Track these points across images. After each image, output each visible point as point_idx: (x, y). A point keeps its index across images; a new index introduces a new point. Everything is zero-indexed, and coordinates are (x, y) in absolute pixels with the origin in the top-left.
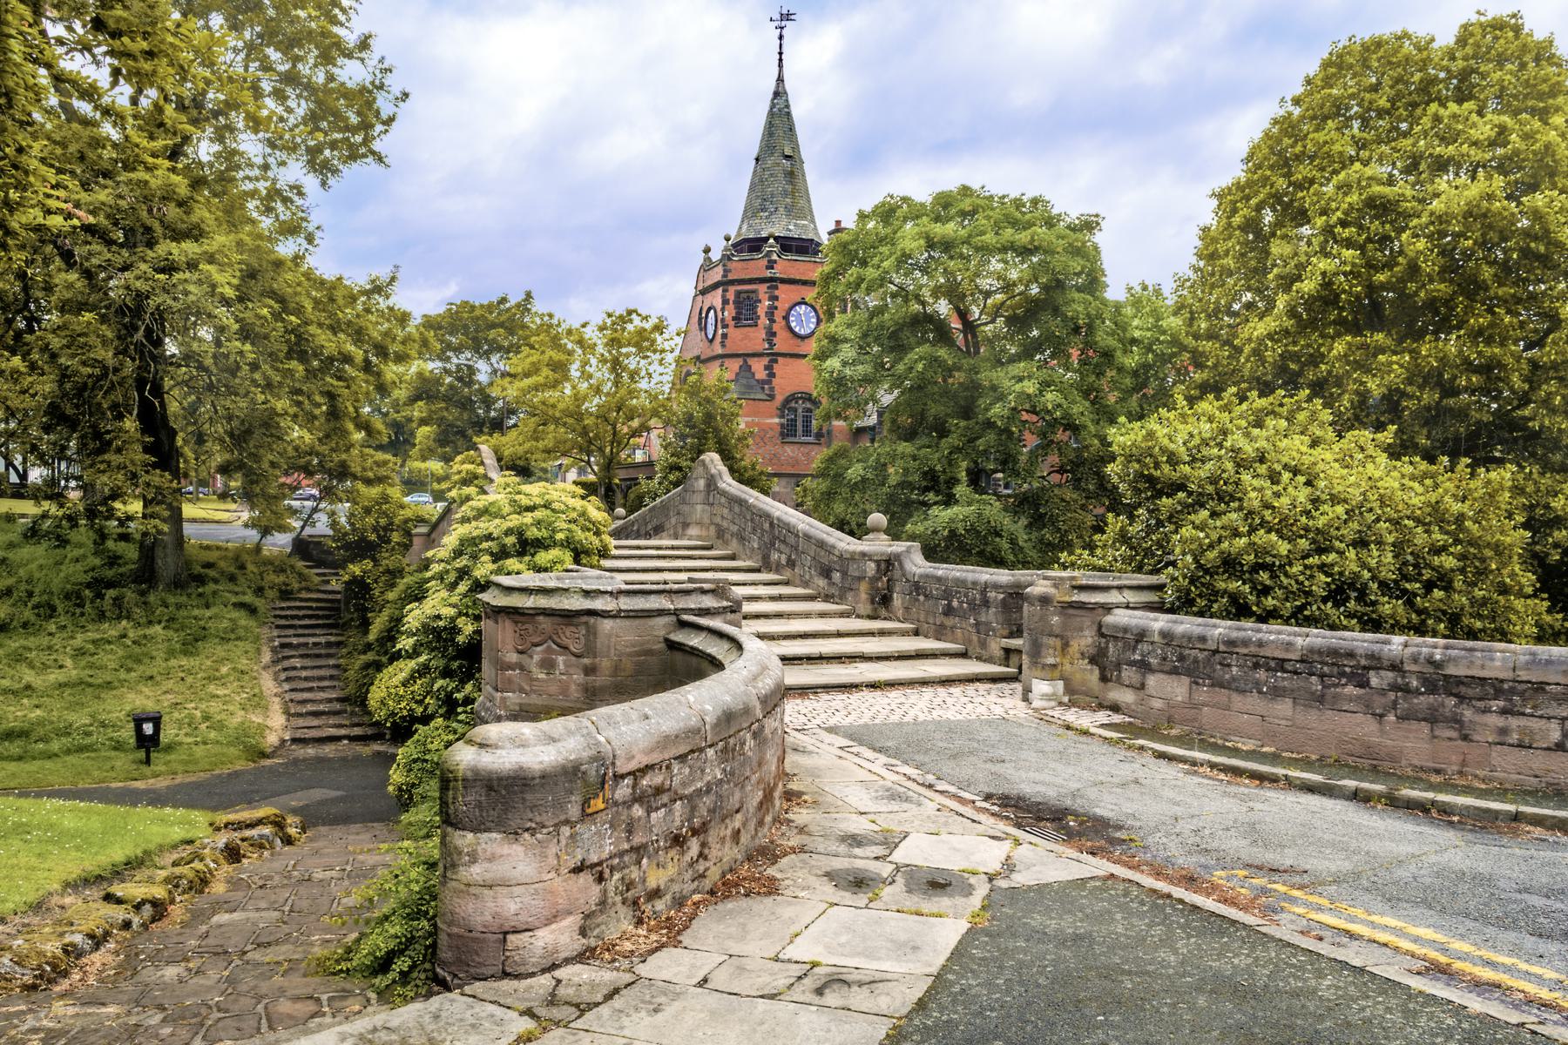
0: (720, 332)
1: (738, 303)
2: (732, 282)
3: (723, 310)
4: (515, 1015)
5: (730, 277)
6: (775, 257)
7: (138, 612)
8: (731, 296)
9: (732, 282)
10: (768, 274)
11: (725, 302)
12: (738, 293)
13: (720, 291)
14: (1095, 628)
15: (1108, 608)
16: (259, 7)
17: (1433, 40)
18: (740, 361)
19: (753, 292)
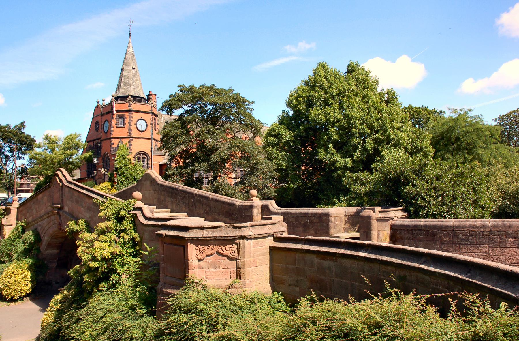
19: (124, 115)
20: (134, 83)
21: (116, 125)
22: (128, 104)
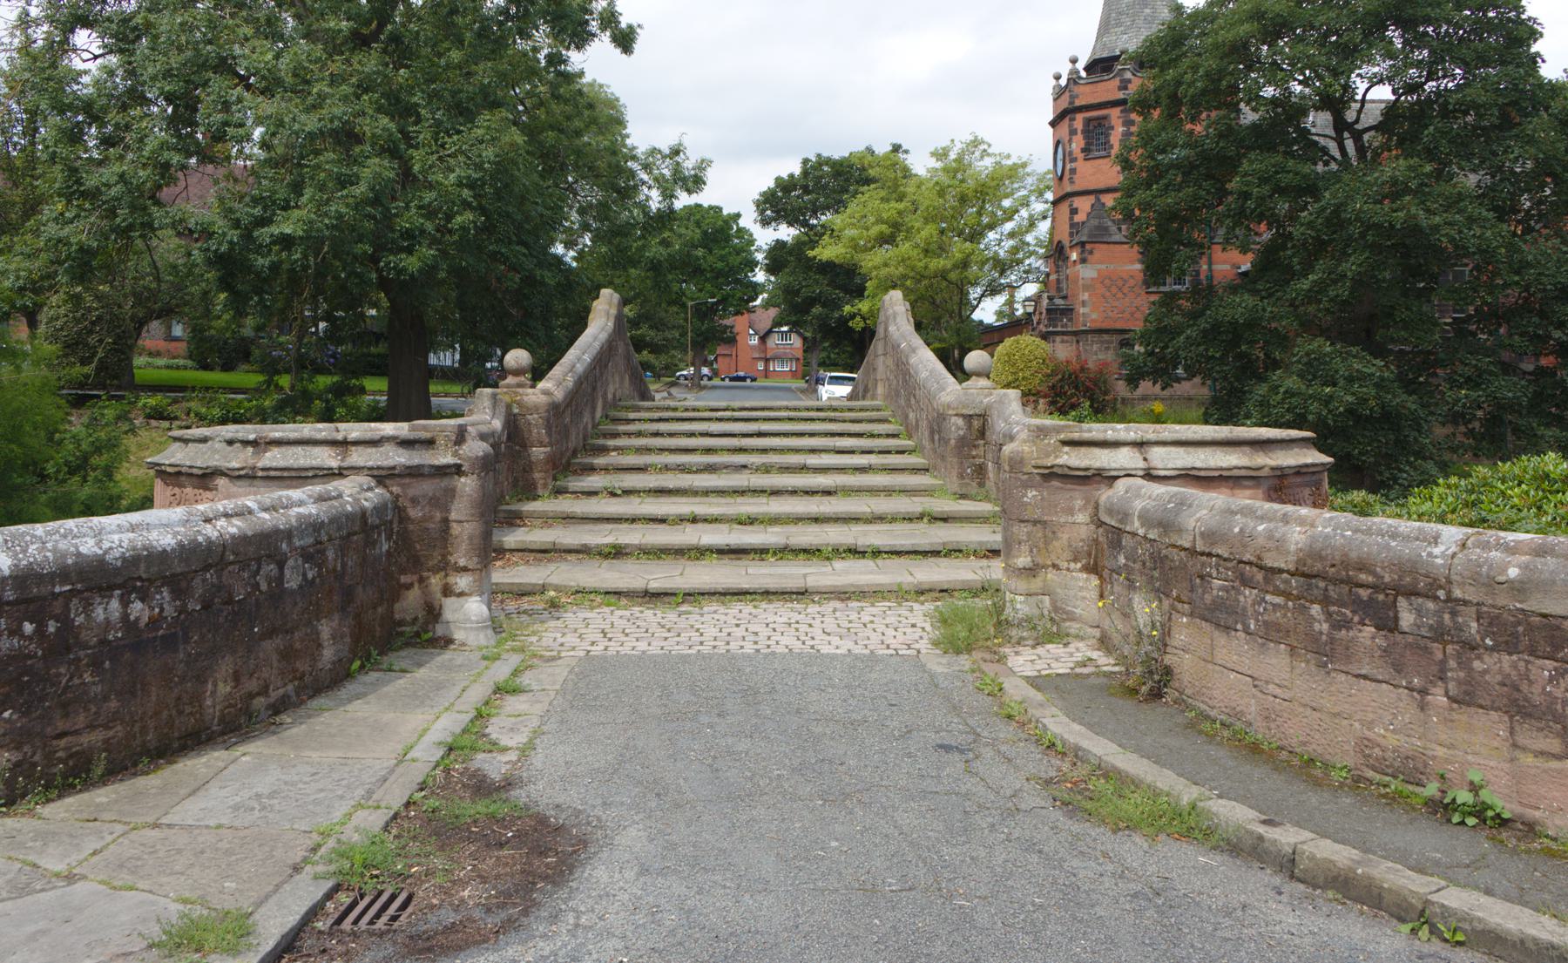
0: (1068, 167)
1: (1086, 132)
2: (1080, 109)
3: (1070, 141)
4: (1140, 481)
5: (1078, 103)
6: (1128, 75)
7: (493, 711)
8: (1079, 123)
9: (1080, 109)
10: (1121, 95)
11: (1073, 132)
12: (1088, 121)
13: (1066, 120)
14: (1090, 510)
15: (1105, 478)
16: (1564, 366)
17: (906, 152)
18: (1091, 199)
19: (1105, 118)
20: (1147, 11)
21: (1083, 150)
22: (1117, 82)
